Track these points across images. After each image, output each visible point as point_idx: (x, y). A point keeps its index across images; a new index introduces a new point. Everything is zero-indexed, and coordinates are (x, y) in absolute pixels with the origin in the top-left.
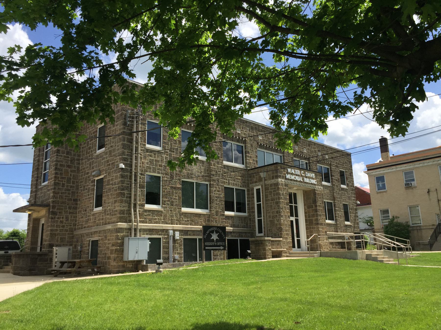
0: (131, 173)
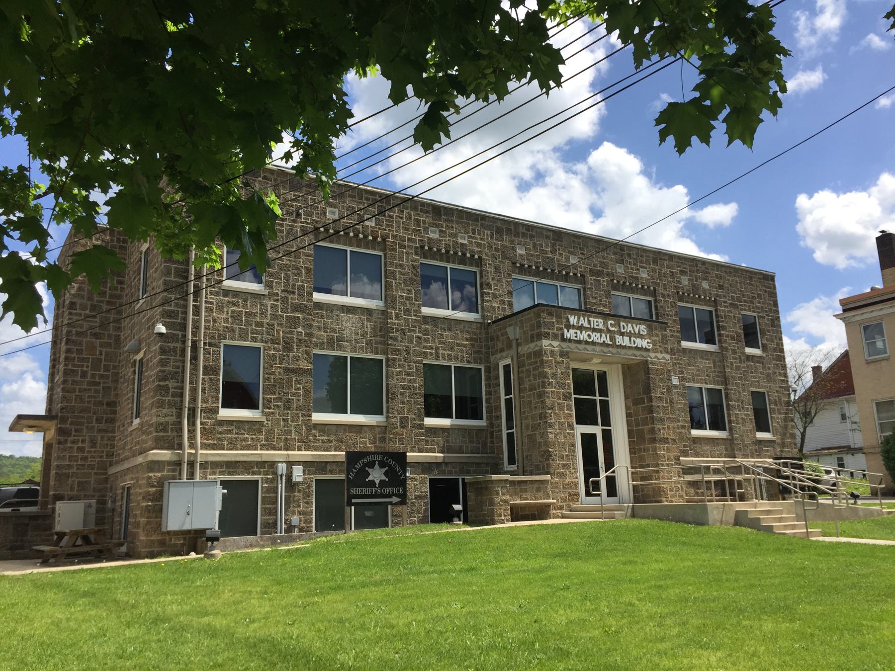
0: (184, 342)
